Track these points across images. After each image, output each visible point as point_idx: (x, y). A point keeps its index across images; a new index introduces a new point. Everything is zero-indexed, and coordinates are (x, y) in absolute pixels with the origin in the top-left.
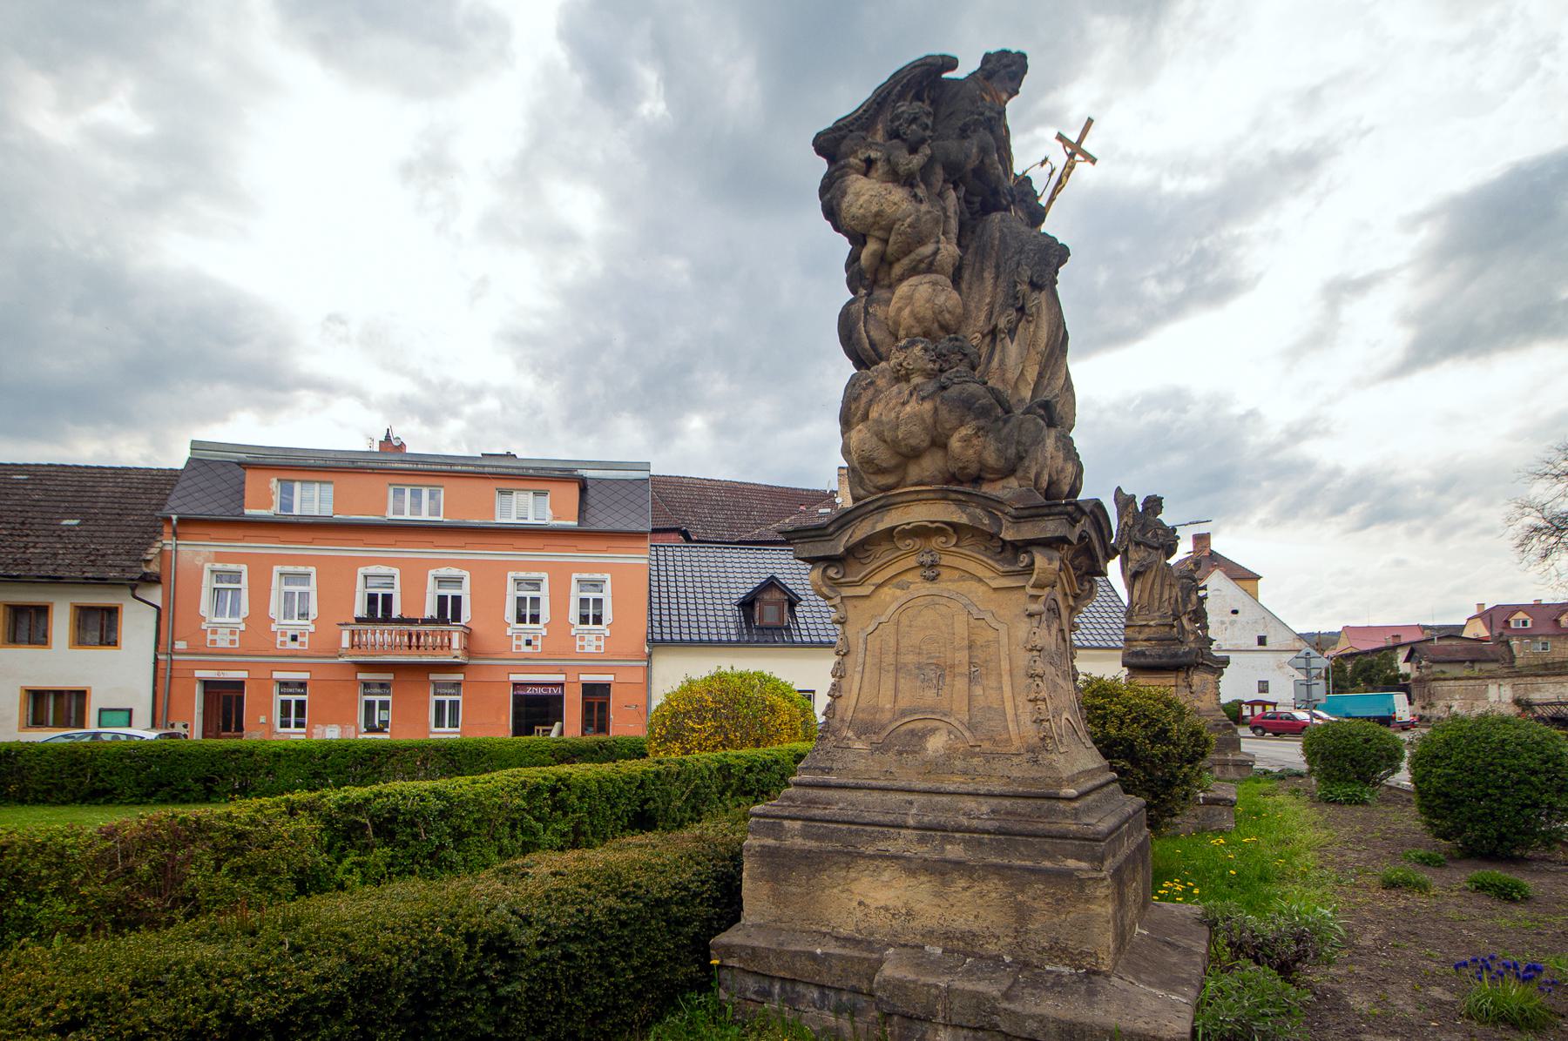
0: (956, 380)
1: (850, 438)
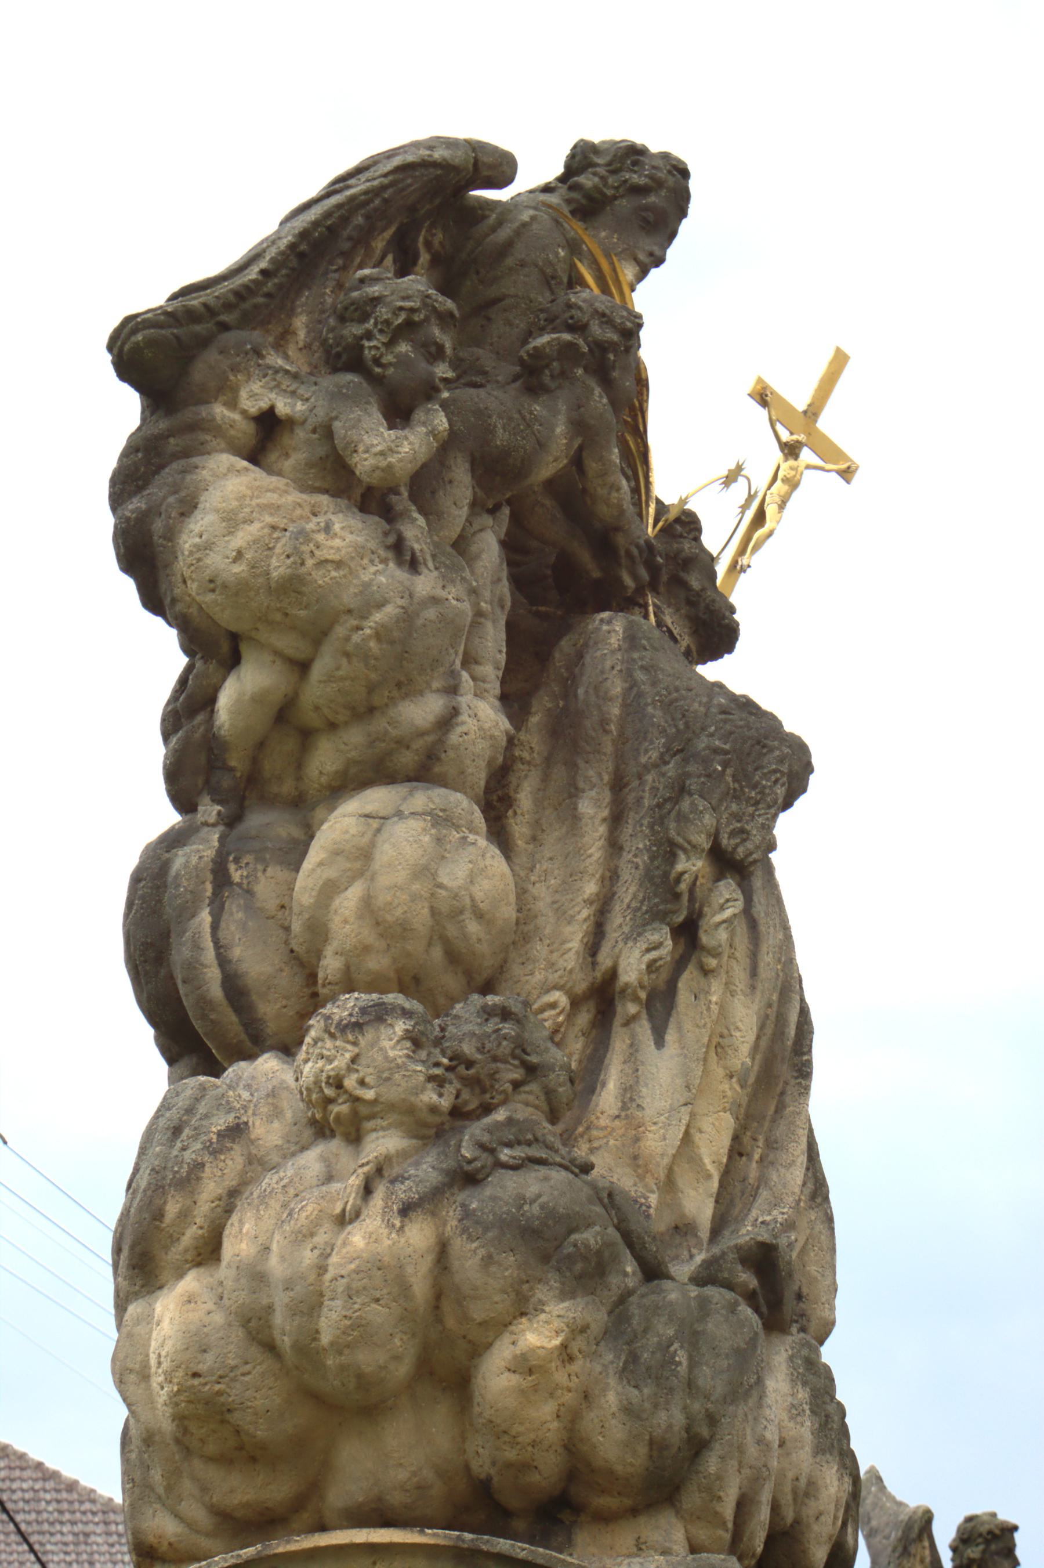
0: (505, 1154)
1: (148, 1318)
